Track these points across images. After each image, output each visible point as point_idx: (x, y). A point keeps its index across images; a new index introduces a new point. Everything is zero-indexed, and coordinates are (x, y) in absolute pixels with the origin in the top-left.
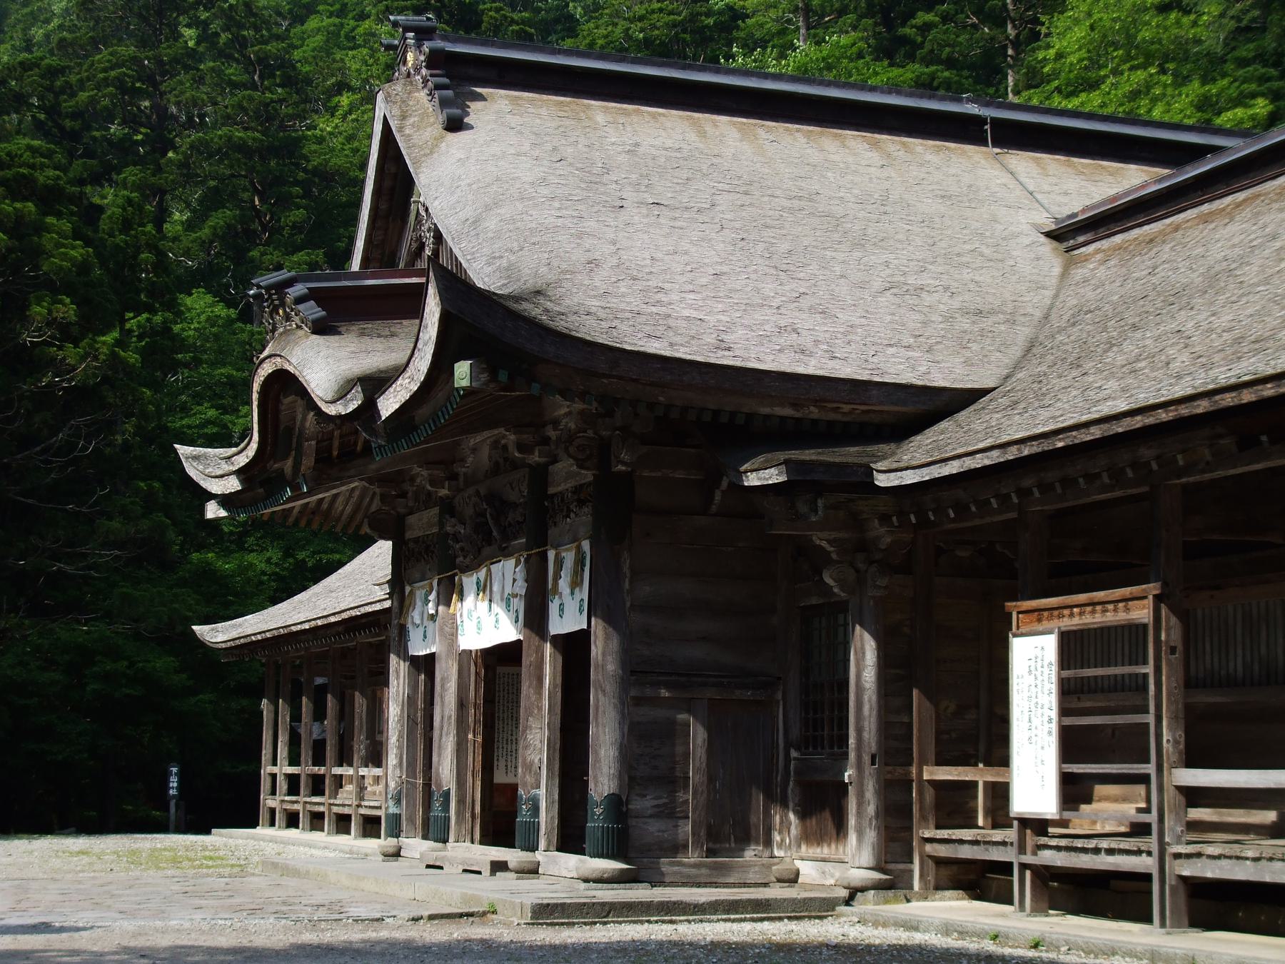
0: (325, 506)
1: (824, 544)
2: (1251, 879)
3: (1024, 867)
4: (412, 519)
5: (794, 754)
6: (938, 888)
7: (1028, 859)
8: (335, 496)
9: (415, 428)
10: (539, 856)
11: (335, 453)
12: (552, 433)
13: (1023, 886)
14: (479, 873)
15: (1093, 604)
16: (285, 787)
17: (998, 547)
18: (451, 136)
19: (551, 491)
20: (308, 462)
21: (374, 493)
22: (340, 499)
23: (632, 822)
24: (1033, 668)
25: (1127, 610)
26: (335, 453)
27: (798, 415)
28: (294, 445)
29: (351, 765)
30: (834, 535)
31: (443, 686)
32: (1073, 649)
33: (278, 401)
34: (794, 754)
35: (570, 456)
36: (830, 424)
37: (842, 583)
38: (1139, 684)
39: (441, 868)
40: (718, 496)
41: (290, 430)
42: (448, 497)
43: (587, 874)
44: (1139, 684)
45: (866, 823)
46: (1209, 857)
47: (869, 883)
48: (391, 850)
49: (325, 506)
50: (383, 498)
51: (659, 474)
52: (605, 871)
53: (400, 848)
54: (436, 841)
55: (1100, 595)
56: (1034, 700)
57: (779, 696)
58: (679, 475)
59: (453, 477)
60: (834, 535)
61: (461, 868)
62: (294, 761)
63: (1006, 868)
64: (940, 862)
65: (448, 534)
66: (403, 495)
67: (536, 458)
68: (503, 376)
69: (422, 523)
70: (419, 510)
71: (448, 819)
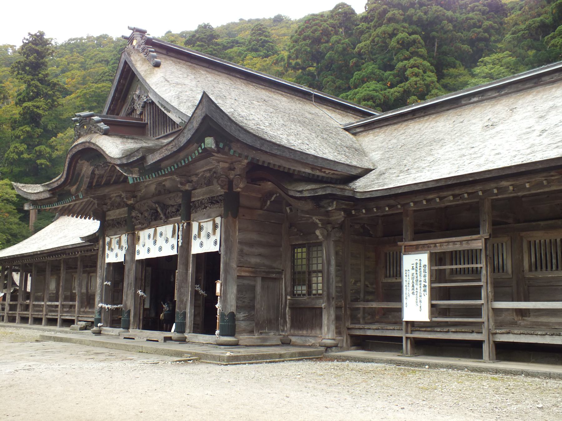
0: (71, 207)
1: (317, 221)
2: (550, 343)
3: (407, 338)
4: (110, 213)
5: (289, 297)
6: (351, 346)
7: (409, 335)
8: (76, 204)
9: (160, 169)
10: (186, 335)
11: (94, 184)
12: (195, 179)
13: (406, 345)
14: (157, 341)
15: (448, 242)
16: (8, 308)
17: (366, 225)
18: (156, 69)
19: (193, 200)
20: (84, 187)
21: (94, 203)
22: (77, 205)
23: (236, 323)
24: (414, 267)
25: (468, 243)
26: (94, 184)
27: (313, 173)
28: (79, 180)
29: (43, 301)
30: (321, 218)
31: (129, 272)
32: (437, 259)
33: (77, 162)
34: (289, 297)
35: (219, 184)
36: (323, 177)
37: (322, 234)
38: (477, 271)
39: (134, 339)
40: (268, 203)
41: (79, 174)
42: (132, 204)
43: (219, 342)
44: (477, 271)
45: (331, 322)
46: (452, 332)
47: (333, 345)
48: (97, 332)
49: (71, 207)
50: (98, 204)
51: (247, 194)
52: (230, 341)
53: (101, 331)
54: (123, 328)
55: (454, 239)
56: (415, 279)
57: (283, 276)
58: (254, 195)
59: (135, 197)
60: (321, 218)
61: (146, 339)
62: (475, 293)
63: (400, 339)
64: (352, 336)
65: (132, 217)
66: (106, 204)
67: (188, 187)
68: (221, 145)
69: (113, 215)
70: (113, 209)
71: (129, 321)
